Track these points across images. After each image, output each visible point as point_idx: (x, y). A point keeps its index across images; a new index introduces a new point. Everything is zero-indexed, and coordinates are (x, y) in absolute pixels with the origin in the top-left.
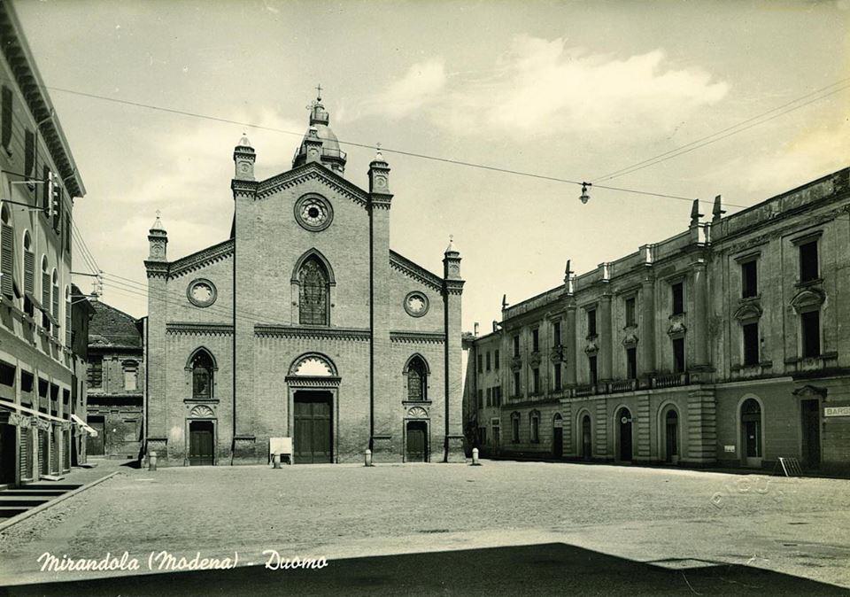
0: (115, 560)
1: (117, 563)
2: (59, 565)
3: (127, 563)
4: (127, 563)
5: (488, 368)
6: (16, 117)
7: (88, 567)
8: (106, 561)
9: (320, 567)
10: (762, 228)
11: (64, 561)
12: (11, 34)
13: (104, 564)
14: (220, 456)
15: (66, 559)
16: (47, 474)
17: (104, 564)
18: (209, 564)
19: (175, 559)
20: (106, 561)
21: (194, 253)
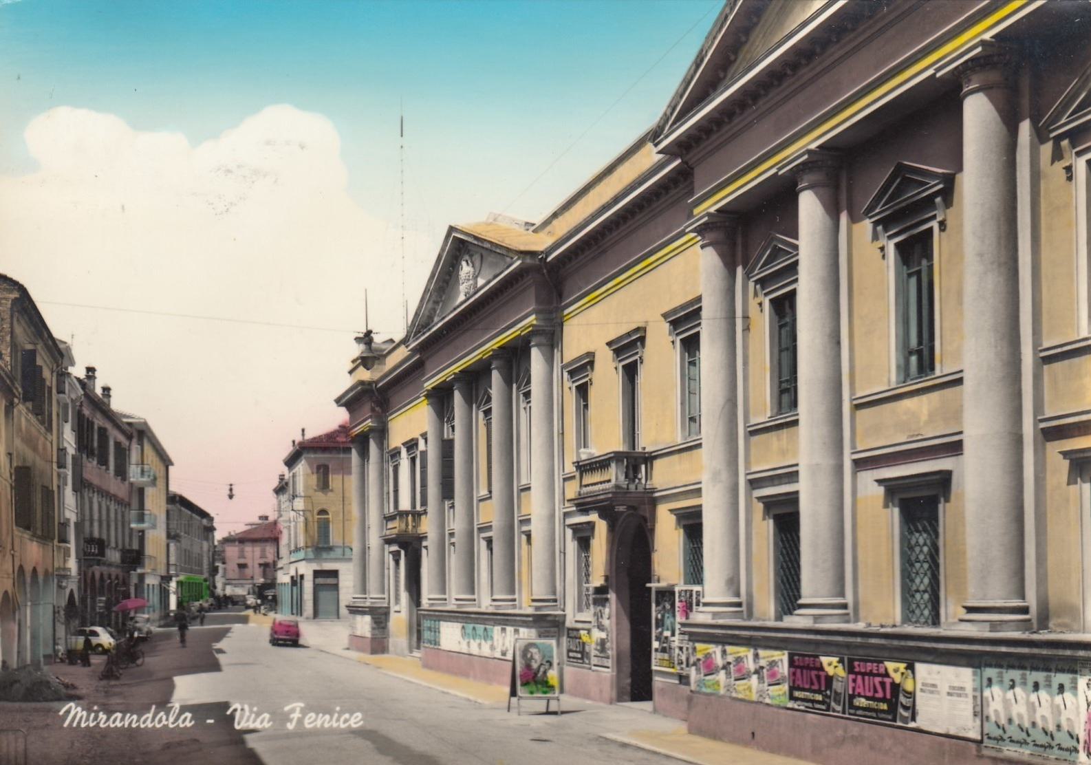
0: (162, 714)
1: (164, 718)
2: (87, 719)
3: (177, 719)
4: (177, 719)
5: (354, 598)
6: (72, 446)
7: (319, 723)
8: (150, 715)
9: (158, 726)
10: (871, 712)
11: (93, 715)
12: (713, 666)
13: (186, 718)
14: (288, 583)
15: (97, 712)
16: (895, 721)
17: (186, 718)
18: (315, 720)
19: (85, 713)
20: (150, 715)
21: (914, 733)
